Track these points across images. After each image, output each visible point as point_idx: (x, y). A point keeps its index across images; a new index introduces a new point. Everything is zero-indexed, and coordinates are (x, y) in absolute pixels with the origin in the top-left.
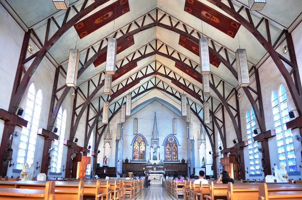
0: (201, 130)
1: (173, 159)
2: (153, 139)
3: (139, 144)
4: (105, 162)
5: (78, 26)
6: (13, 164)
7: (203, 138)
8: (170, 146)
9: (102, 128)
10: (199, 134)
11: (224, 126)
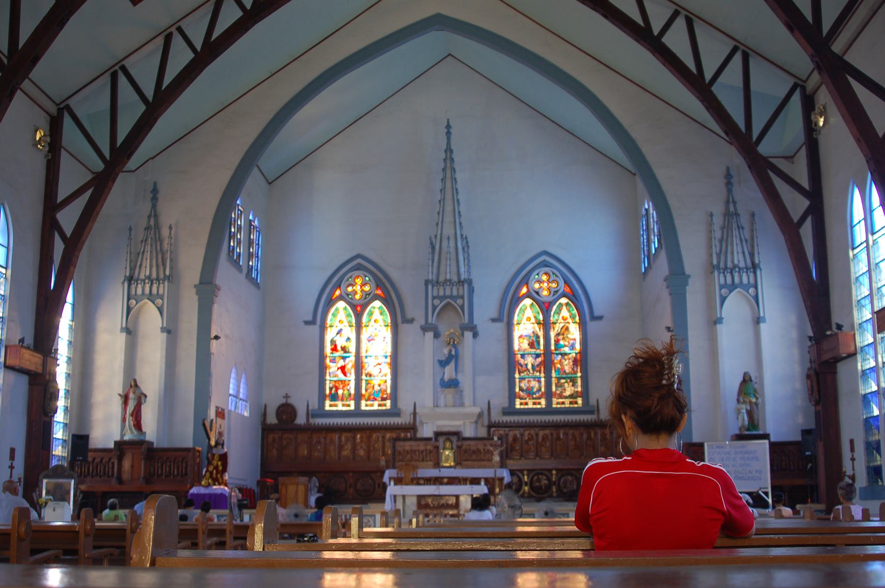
1: (561, 396)
3: (359, 316)
6: (18, 480)
7: (739, 259)
10: (718, 234)
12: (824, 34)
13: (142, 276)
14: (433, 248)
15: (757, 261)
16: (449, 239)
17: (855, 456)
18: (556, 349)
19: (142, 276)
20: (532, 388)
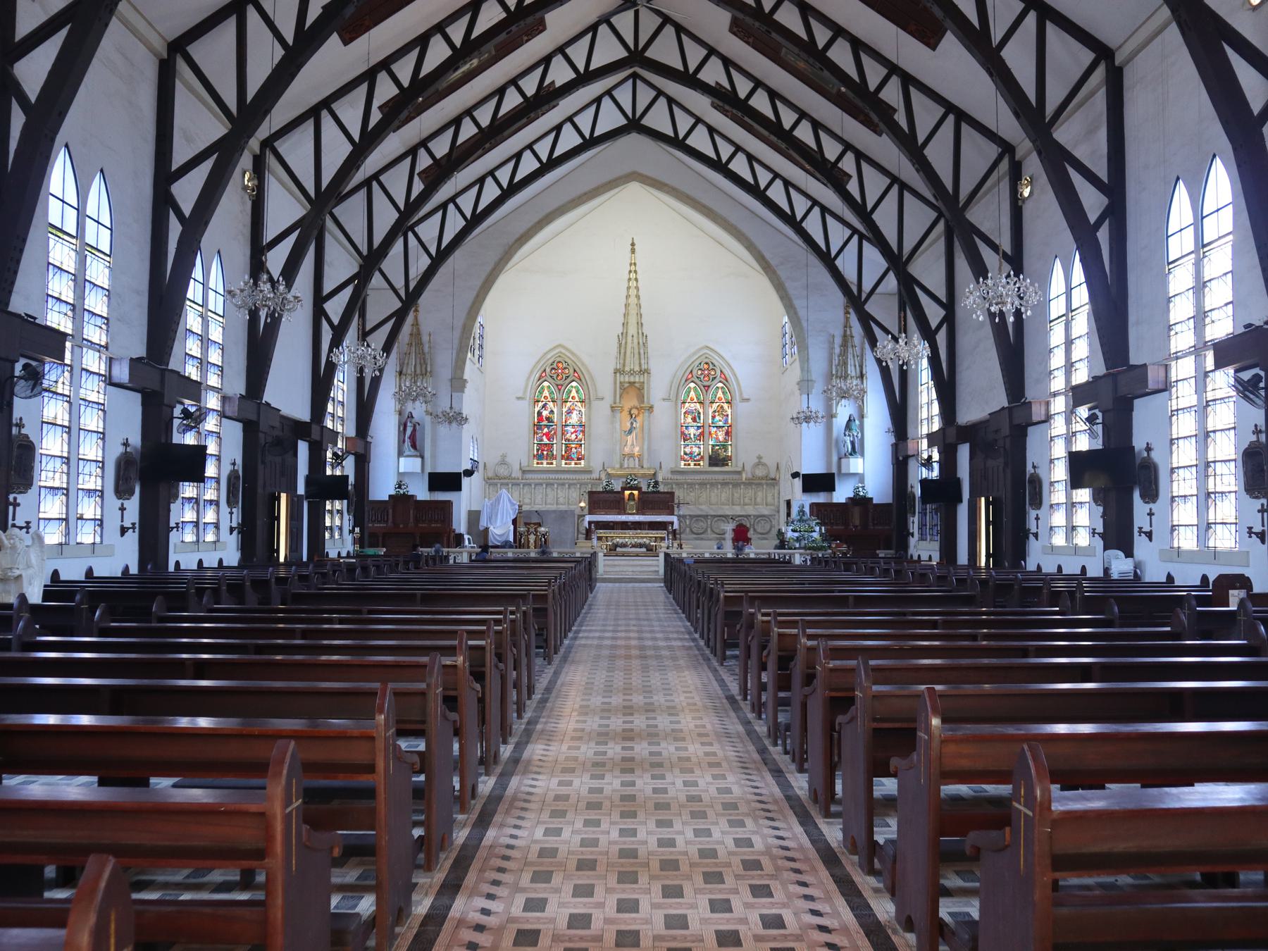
0: (845, 331)
4: (408, 443)
9: (388, 327)
10: (837, 350)
11: (950, 319)
14: (620, 345)
15: (864, 372)
18: (712, 423)
19: (409, 372)
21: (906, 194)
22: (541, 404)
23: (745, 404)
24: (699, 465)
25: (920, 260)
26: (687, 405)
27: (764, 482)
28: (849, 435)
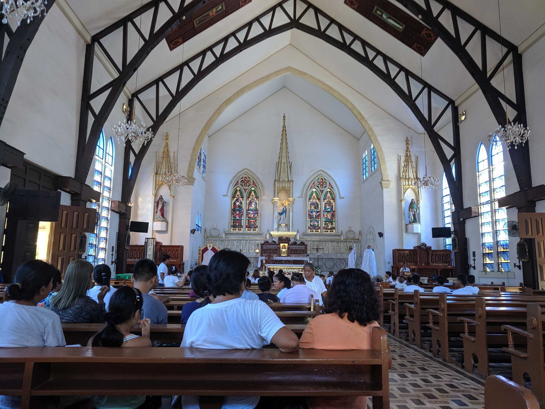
2: (279, 181)
4: (159, 213)
5: (173, 43)
8: (319, 199)
10: (403, 164)
12: (488, 77)
13: (161, 173)
16: (284, 163)
17: (476, 258)
18: (325, 210)
20: (315, 225)
21: (432, 93)
22: (235, 199)
23: (341, 200)
24: (318, 231)
25: (496, 77)
26: (311, 200)
27: (353, 241)
28: (412, 211)
